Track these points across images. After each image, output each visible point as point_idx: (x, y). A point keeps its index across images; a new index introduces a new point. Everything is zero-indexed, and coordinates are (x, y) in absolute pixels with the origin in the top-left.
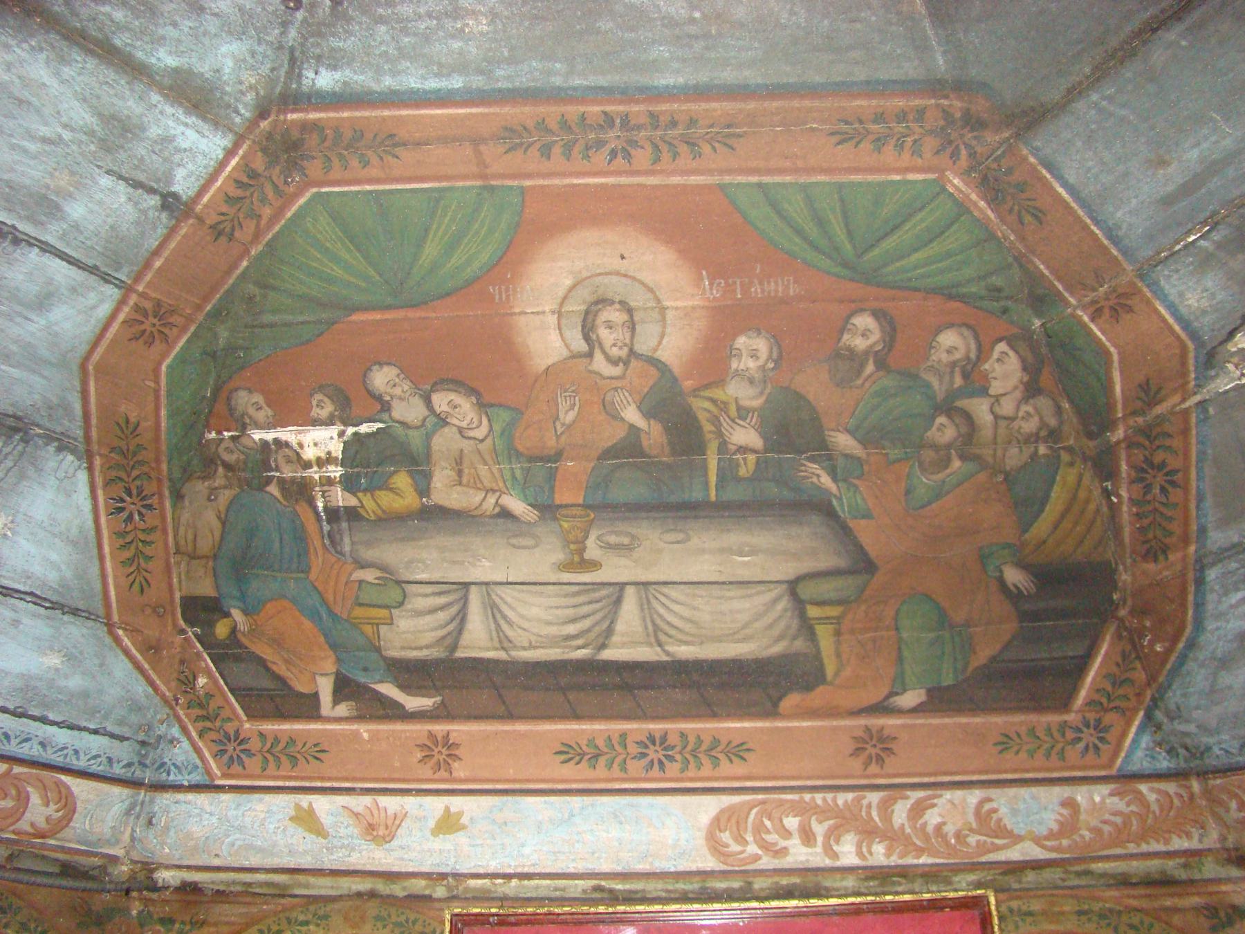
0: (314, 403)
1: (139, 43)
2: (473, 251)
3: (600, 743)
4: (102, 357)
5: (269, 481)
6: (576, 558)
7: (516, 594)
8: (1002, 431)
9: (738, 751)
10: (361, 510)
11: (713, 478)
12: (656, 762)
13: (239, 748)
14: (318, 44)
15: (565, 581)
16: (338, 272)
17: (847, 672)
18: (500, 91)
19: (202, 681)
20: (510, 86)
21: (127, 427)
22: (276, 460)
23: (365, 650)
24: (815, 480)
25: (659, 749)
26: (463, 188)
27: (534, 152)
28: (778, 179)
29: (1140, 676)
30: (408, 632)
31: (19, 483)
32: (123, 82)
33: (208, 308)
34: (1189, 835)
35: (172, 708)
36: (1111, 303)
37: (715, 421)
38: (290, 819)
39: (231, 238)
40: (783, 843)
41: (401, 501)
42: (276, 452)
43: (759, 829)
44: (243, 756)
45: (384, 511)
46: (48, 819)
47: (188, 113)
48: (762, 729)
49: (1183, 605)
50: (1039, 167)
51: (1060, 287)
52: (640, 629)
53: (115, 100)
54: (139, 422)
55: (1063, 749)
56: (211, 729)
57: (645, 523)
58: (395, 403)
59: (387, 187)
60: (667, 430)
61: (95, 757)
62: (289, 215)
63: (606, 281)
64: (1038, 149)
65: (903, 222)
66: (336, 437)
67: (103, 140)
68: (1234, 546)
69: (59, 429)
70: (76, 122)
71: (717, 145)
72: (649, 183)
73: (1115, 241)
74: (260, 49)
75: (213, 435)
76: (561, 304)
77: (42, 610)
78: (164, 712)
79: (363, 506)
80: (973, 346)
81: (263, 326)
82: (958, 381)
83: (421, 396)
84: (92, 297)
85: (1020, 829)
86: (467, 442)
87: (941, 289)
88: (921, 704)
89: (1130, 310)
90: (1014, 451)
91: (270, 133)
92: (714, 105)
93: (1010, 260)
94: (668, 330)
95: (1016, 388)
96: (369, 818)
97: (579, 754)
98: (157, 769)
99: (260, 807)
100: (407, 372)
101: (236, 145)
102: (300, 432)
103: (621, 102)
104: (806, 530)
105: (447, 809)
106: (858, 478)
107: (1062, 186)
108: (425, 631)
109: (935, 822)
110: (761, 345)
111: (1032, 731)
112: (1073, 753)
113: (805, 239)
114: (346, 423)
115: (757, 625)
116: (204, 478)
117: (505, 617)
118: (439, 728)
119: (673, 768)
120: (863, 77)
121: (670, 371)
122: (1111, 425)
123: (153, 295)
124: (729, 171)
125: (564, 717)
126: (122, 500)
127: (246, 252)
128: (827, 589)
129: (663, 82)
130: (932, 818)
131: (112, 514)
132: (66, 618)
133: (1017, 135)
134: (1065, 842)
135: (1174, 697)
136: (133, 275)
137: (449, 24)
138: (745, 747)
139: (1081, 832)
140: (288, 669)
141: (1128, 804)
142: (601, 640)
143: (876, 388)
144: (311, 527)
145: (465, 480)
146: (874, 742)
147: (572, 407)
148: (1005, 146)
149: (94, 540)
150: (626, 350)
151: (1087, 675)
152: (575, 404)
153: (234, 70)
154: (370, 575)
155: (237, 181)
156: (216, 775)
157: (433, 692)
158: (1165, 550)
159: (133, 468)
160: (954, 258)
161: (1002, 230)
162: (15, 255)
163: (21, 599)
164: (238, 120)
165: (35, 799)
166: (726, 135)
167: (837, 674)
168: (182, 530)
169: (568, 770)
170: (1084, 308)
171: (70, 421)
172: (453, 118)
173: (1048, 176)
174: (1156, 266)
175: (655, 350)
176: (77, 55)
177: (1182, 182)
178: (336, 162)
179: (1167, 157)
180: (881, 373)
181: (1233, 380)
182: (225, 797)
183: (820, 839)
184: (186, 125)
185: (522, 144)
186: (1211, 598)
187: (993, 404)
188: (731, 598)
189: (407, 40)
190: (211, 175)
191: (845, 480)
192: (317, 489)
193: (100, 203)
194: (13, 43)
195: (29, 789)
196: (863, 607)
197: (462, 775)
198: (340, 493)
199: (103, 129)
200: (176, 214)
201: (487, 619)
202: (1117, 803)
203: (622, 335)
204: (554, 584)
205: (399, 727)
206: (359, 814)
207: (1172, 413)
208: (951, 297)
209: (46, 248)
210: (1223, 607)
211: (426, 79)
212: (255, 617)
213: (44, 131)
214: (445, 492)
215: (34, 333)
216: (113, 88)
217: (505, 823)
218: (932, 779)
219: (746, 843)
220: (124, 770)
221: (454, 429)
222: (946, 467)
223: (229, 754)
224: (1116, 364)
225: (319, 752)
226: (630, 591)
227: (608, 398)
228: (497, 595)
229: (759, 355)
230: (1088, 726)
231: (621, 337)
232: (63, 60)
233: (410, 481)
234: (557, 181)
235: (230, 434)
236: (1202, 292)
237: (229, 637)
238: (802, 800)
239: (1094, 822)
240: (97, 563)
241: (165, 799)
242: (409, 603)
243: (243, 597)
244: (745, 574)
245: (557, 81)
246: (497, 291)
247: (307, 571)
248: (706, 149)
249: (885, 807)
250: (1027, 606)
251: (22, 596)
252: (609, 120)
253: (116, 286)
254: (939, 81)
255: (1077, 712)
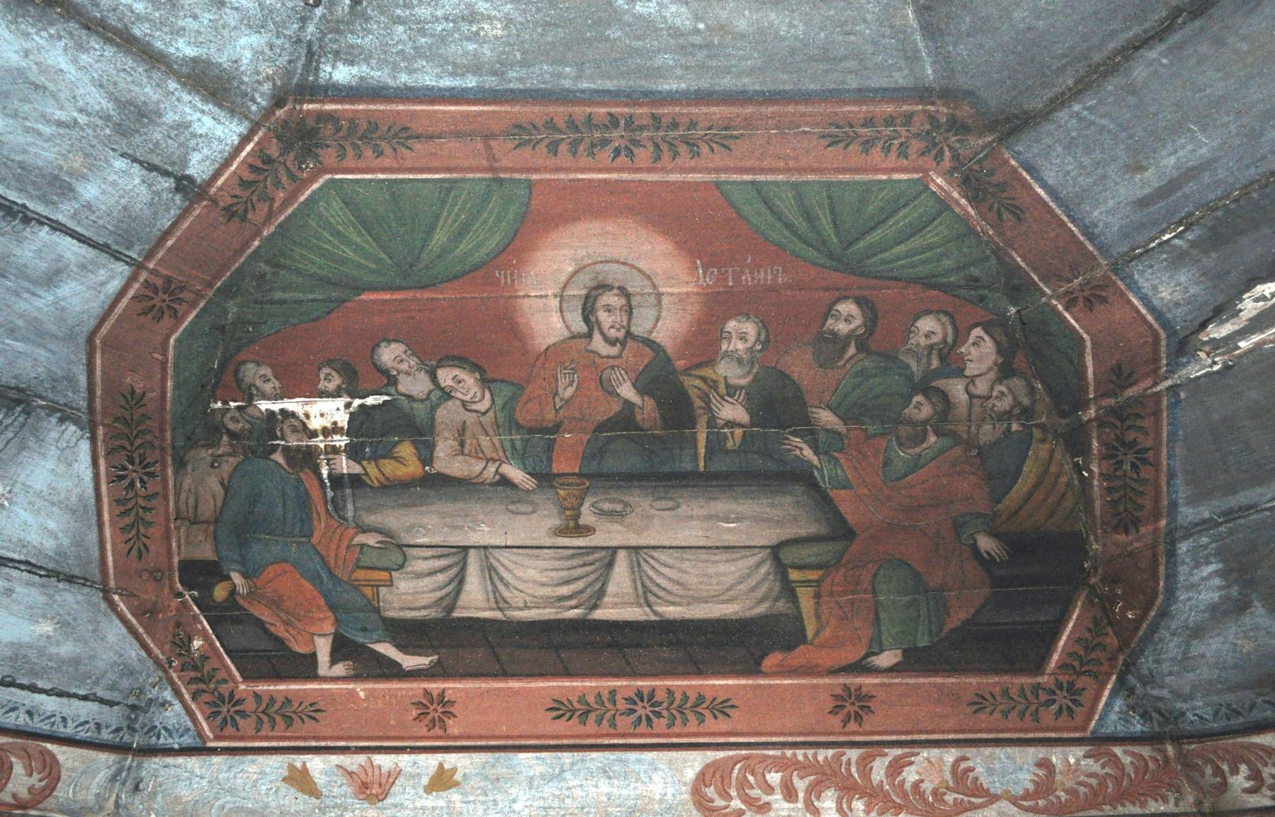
0: (322, 376)
1: (158, 33)
2: (481, 238)
3: (591, 699)
4: (110, 331)
5: (274, 449)
6: (571, 524)
7: (514, 558)
8: (976, 409)
9: (722, 708)
10: (364, 478)
11: (702, 451)
12: (644, 718)
13: (232, 710)
14: (336, 40)
15: (561, 545)
16: (349, 253)
17: (827, 633)
18: (512, 91)
19: (197, 643)
20: (521, 86)
21: (133, 399)
22: (282, 430)
23: (364, 611)
24: (798, 452)
25: (647, 706)
26: (472, 180)
27: (542, 148)
28: (770, 178)
29: (1112, 641)
30: (407, 594)
31: (19, 453)
32: (140, 70)
33: (219, 284)
34: (1165, 800)
35: (165, 671)
36: (1086, 294)
37: (706, 398)
38: (283, 780)
39: (244, 218)
40: (766, 798)
41: (405, 470)
42: (282, 422)
43: (743, 785)
44: (237, 718)
45: (387, 479)
46: (31, 789)
47: (205, 100)
48: (745, 686)
49: (1155, 576)
50: (1020, 170)
51: (1036, 279)
52: (631, 590)
53: (133, 87)
54: (144, 393)
55: (1037, 711)
56: (204, 691)
57: (637, 492)
58: (401, 377)
59: (400, 176)
60: (660, 405)
61: (82, 724)
62: (302, 199)
63: (606, 268)
64: (1019, 153)
65: (887, 219)
66: (342, 408)
67: (118, 124)
68: (1204, 522)
69: (62, 400)
70: (92, 107)
71: (714, 146)
72: (649, 179)
73: (1091, 237)
74: (279, 42)
75: (219, 404)
76: (564, 288)
77: (37, 578)
78: (157, 675)
79: (367, 474)
80: (950, 331)
81: (272, 302)
82: (935, 363)
83: (427, 371)
84: (102, 274)
85: (997, 789)
86: (469, 414)
87: (921, 278)
88: (896, 665)
89: (1104, 300)
90: (988, 427)
91: (286, 122)
92: (714, 109)
93: (988, 252)
94: (664, 314)
95: (990, 369)
96: (363, 776)
97: (570, 711)
98: (146, 734)
99: (252, 769)
100: (415, 349)
101: (252, 132)
102: (307, 403)
103: (626, 105)
104: (789, 499)
105: (441, 766)
106: (840, 451)
107: (1040, 187)
108: (424, 592)
109: (913, 780)
110: (750, 328)
111: (1006, 692)
112: (1047, 716)
113: (795, 233)
114: (353, 395)
115: (742, 587)
116: (207, 446)
117: (501, 579)
118: (435, 686)
119: (660, 724)
120: (854, 86)
121: (664, 351)
122: (1084, 405)
123: (164, 272)
124: (726, 170)
125: (555, 675)
126: (125, 468)
127: (258, 233)
128: (808, 553)
129: (666, 87)
130: (910, 775)
131: (113, 481)
132: (61, 585)
133: (1000, 140)
134: (1041, 803)
135: (1146, 663)
136: (144, 253)
137: (465, 27)
138: (728, 704)
139: (1057, 793)
140: (287, 631)
141: (1103, 767)
142: (593, 601)
143: (858, 368)
144: (315, 493)
145: (466, 451)
146: (853, 699)
147: (571, 384)
148: (987, 149)
149: (94, 508)
150: (623, 331)
151: (1060, 639)
152: (573, 381)
153: (252, 61)
154: (371, 540)
155: (251, 166)
156: (208, 737)
157: (430, 651)
158: (1137, 523)
159: (136, 437)
160: (934, 251)
161: (980, 225)
162: (25, 233)
163: (15, 568)
164: (254, 108)
165: (18, 769)
166: (724, 137)
167: (817, 634)
168: (183, 496)
169: (561, 726)
170: (1058, 298)
171: (74, 393)
172: (466, 115)
173: (1028, 178)
174: (1131, 261)
175: (651, 332)
176: (95, 43)
177: (1158, 185)
178: (350, 152)
179: (1145, 163)
180: (861, 356)
181: (1204, 367)
182: (216, 759)
183: (801, 795)
184: (203, 112)
185: (531, 140)
186: (1183, 570)
187: (968, 384)
188: (717, 562)
189: (423, 40)
190: (226, 159)
191: (826, 453)
192: (322, 457)
193: (114, 184)
194: (32, 31)
195: (13, 759)
196: (842, 571)
197: (456, 731)
198: (344, 462)
199: (119, 114)
200: (190, 196)
201: (485, 580)
202: (1092, 765)
203: (619, 318)
204: (549, 548)
205: (395, 685)
206: (353, 772)
207: (1142, 396)
208: (932, 287)
209: (57, 227)
210: (1195, 579)
211: (441, 78)
212: (255, 580)
213: (60, 115)
214: (447, 461)
215: (42, 308)
216: (131, 75)
217: (498, 779)
218: (909, 738)
219: (730, 798)
220: (112, 736)
221: (458, 403)
222: (923, 441)
223: (222, 715)
224: (1088, 350)
225: (314, 711)
226: (622, 554)
227: (605, 376)
228: (495, 558)
229: (748, 337)
230: (1061, 689)
231: (619, 319)
232: (81, 47)
233: (413, 450)
234: (562, 176)
235: (236, 404)
236: (1175, 286)
237: (226, 600)
238: (784, 757)
239: (1070, 784)
240: (95, 529)
241: (155, 763)
242: (410, 565)
243: (243, 561)
244: (731, 539)
245: (567, 84)
246: (502, 276)
247: (310, 536)
248: (705, 149)
249: (864, 764)
250: (1001, 572)
251: (17, 565)
252: (614, 121)
253: (127, 263)
254: (927, 89)
255: (1050, 675)
